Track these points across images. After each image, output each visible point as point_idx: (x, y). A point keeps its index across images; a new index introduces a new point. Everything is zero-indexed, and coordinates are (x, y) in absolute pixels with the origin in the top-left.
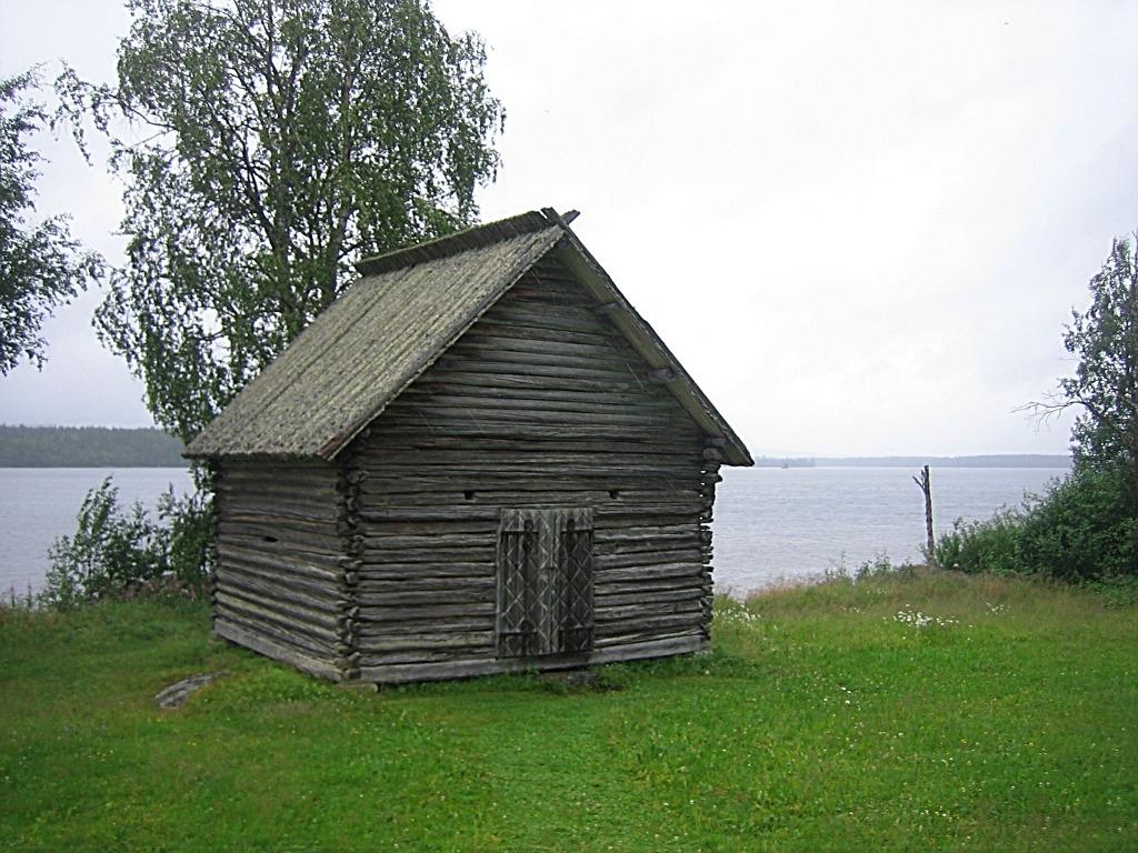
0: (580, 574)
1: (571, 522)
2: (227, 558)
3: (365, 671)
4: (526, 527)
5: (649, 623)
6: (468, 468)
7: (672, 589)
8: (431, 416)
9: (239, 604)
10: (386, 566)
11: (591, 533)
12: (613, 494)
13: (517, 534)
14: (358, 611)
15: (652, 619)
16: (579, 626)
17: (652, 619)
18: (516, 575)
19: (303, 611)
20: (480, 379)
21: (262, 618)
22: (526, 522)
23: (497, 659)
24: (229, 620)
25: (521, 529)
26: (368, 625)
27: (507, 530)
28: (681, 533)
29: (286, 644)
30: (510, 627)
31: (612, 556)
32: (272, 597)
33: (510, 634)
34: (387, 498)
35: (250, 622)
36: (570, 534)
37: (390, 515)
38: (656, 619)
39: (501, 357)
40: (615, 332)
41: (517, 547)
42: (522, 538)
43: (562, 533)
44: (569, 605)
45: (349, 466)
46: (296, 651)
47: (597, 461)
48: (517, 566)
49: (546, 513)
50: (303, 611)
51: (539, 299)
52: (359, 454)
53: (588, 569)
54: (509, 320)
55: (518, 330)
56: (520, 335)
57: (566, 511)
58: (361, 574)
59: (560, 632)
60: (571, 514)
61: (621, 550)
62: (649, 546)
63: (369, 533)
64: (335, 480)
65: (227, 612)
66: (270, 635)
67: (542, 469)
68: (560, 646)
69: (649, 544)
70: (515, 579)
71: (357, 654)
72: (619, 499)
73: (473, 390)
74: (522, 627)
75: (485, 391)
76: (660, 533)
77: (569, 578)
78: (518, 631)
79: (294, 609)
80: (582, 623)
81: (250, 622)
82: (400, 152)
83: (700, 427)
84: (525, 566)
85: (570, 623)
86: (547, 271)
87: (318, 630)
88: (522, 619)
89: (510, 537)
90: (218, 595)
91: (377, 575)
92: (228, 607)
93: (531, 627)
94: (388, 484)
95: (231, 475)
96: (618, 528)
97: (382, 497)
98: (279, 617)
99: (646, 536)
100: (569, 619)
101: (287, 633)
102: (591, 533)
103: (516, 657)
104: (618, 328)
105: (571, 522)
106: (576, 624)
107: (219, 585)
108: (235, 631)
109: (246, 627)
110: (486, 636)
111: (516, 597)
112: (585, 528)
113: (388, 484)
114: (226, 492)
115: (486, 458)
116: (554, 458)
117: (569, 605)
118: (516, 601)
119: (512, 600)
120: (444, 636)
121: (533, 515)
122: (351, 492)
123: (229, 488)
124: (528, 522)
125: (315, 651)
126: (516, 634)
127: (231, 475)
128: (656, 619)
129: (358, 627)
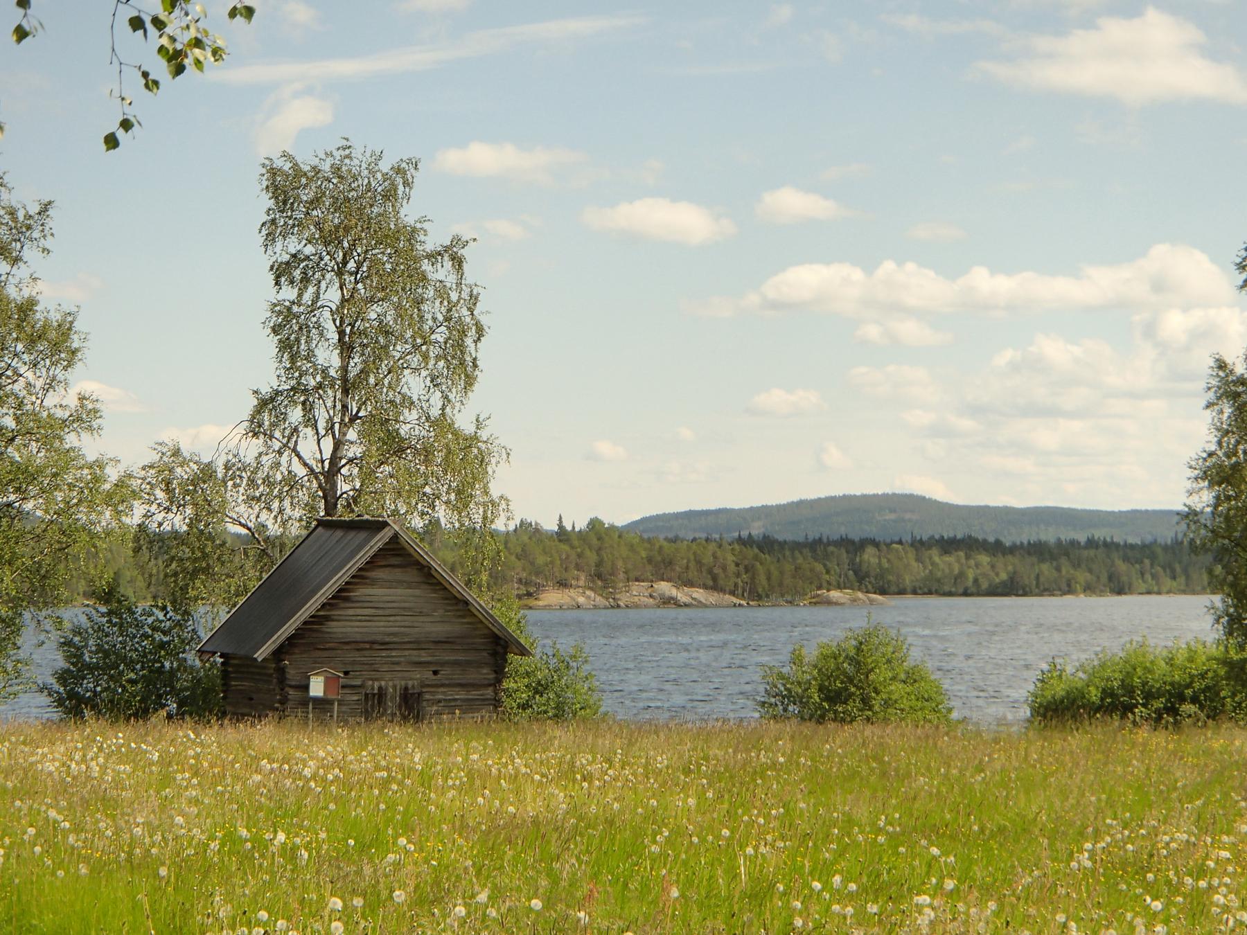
12: (435, 673)
13: (374, 695)
49: (391, 683)
55: (374, 583)
105: (406, 689)
115: (357, 654)
124: (380, 688)
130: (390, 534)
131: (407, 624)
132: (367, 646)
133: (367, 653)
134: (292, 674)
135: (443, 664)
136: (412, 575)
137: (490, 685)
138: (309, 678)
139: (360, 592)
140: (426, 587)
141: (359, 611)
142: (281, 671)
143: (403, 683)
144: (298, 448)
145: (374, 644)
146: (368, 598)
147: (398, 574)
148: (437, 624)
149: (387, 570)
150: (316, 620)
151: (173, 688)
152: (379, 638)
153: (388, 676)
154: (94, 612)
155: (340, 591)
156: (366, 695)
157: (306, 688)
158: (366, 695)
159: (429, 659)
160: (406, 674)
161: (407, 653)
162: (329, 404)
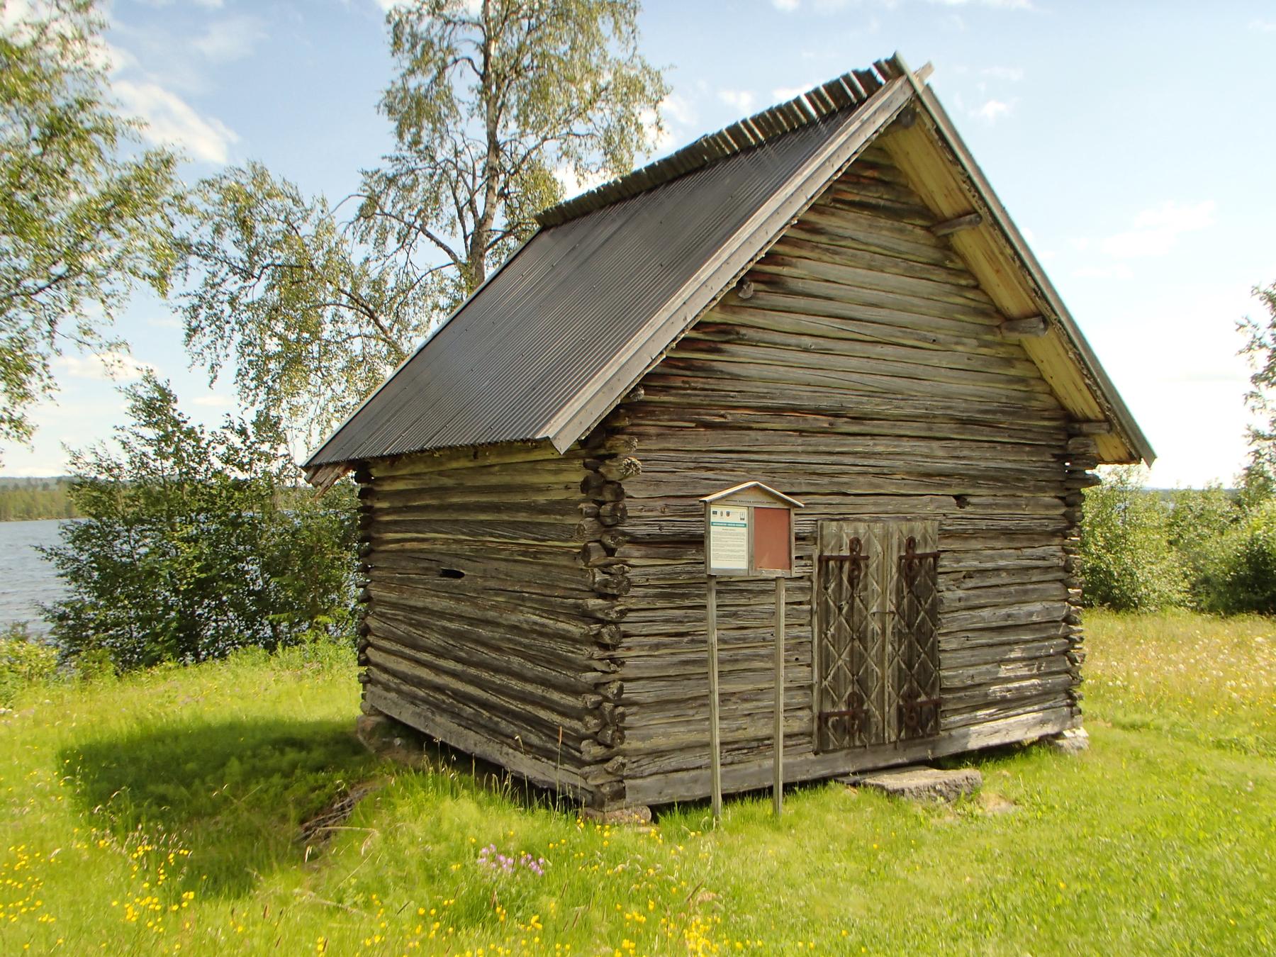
0: (923, 618)
1: (911, 543)
2: (381, 602)
3: (632, 788)
4: (852, 550)
5: (1009, 690)
6: (772, 457)
7: (1033, 641)
8: (735, 377)
9: (404, 667)
10: (659, 613)
11: (936, 556)
12: (961, 500)
13: (842, 560)
14: (621, 689)
15: (1010, 686)
16: (923, 698)
17: (1010, 686)
18: (840, 624)
19: (515, 684)
20: (787, 321)
21: (439, 689)
22: (852, 542)
23: (816, 754)
24: (387, 688)
25: (846, 552)
26: (634, 709)
27: (827, 553)
28: (1044, 559)
29: (482, 731)
30: (834, 704)
31: (960, 593)
32: (458, 660)
33: (834, 714)
34: (661, 503)
35: (421, 693)
36: (910, 566)
37: (664, 532)
38: (1016, 685)
39: (815, 291)
40: (960, 265)
41: (841, 579)
42: (847, 566)
43: (900, 558)
44: (910, 667)
45: (602, 452)
46: (502, 743)
47: (941, 453)
48: (840, 609)
49: (878, 528)
50: (515, 684)
51: (862, 206)
52: (620, 431)
53: (933, 613)
54: (822, 233)
55: (835, 246)
56: (837, 258)
57: (905, 527)
58: (623, 628)
59: (899, 709)
60: (912, 530)
61: (970, 583)
62: (1004, 578)
63: (632, 562)
64: (579, 478)
65: (384, 677)
66: (455, 715)
67: (872, 462)
68: (900, 732)
69: (1004, 574)
70: (839, 628)
71: (620, 759)
72: (968, 509)
73: (778, 338)
74: (849, 703)
75: (793, 340)
76: (1018, 558)
77: (909, 626)
78: (844, 709)
79: (498, 679)
80: (926, 694)
81: (421, 693)
82: (304, 569)
83: (1062, 407)
84: (852, 608)
85: (911, 695)
86: (873, 166)
87: (543, 714)
88: (849, 690)
89: (831, 563)
90: (370, 651)
91: (645, 631)
92: (385, 670)
93: (861, 703)
94: (659, 482)
95: (388, 487)
96: (967, 552)
97: (652, 503)
98: (471, 690)
99: (1002, 563)
100: (911, 687)
101: (486, 714)
102: (936, 556)
103: (842, 749)
104: (963, 258)
105: (911, 543)
106: (919, 695)
107: (370, 638)
108: (396, 704)
109: (413, 699)
110: (801, 719)
111: (840, 656)
112: (928, 551)
113: (659, 482)
114: (381, 510)
115: (797, 443)
116: (888, 446)
117: (910, 667)
118: (840, 662)
119: (835, 662)
120: (742, 722)
121: (861, 531)
122: (608, 496)
123: (385, 505)
124: (855, 543)
125: (538, 748)
126: (840, 714)
127: (388, 487)
128: (1016, 685)
129: (623, 716)
130: (902, 99)
131: (898, 368)
132: (823, 422)
133: (823, 442)
134: (644, 506)
135: (974, 479)
136: (913, 240)
137: (1053, 534)
138: (703, 514)
139: (805, 270)
140: (941, 275)
141: (806, 323)
142: (602, 489)
143: (899, 530)
144: (428, 228)
145: (839, 418)
146: (824, 289)
147: (882, 234)
148: (954, 376)
149: (864, 217)
150: (709, 336)
151: (255, 545)
152: (851, 401)
153: (869, 505)
154: (132, 438)
155: (771, 258)
156: (824, 561)
157: (699, 542)
158: (824, 561)
159: (950, 464)
160: (905, 504)
161: (906, 445)
162: (463, 195)
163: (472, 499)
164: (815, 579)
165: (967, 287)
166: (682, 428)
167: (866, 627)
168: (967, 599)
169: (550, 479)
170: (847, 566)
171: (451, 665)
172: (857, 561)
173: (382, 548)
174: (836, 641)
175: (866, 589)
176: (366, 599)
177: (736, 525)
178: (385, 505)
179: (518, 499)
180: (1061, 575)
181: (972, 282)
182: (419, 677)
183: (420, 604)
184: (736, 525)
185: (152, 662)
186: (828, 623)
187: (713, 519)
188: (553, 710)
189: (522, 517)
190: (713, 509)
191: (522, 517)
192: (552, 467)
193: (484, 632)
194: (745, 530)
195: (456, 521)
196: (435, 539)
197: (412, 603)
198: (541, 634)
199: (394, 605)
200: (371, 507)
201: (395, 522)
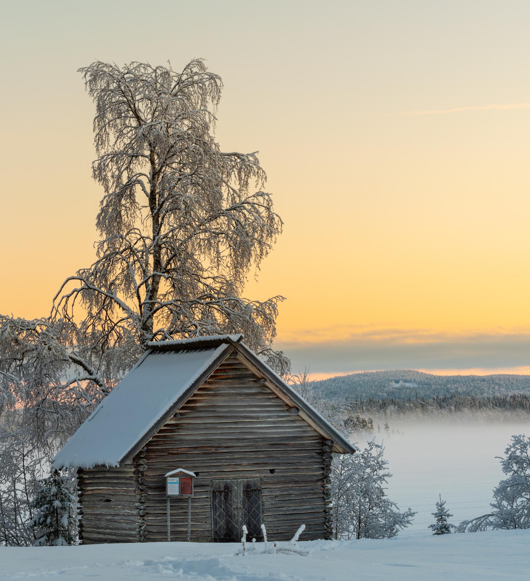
19: (124, 532)
28: (312, 490)
32: (110, 529)
42: (223, 494)
48: (221, 507)
50: (124, 532)
61: (278, 499)
114: (86, 478)
156: (214, 492)
163: (112, 475)
164: (212, 498)
165: (273, 398)
166: (163, 455)
167: (231, 513)
168: (275, 504)
169: (129, 470)
170: (223, 494)
171: (108, 531)
172: (227, 490)
173: (86, 493)
174: (219, 516)
175: (231, 500)
176: (81, 513)
177: (175, 483)
178: (87, 476)
179: (123, 475)
180: (322, 496)
181: (275, 396)
182: (99, 538)
183: (99, 512)
184: (175, 483)
185: (274, 329)
186: (216, 511)
187: (168, 481)
188: (132, 536)
189: (124, 481)
190: (168, 479)
191: (124, 481)
192: (129, 466)
193: (116, 518)
194: (178, 484)
195: (108, 483)
196: (103, 489)
197: (96, 512)
198: (129, 515)
199: (91, 514)
200: (82, 477)
201: (91, 483)
